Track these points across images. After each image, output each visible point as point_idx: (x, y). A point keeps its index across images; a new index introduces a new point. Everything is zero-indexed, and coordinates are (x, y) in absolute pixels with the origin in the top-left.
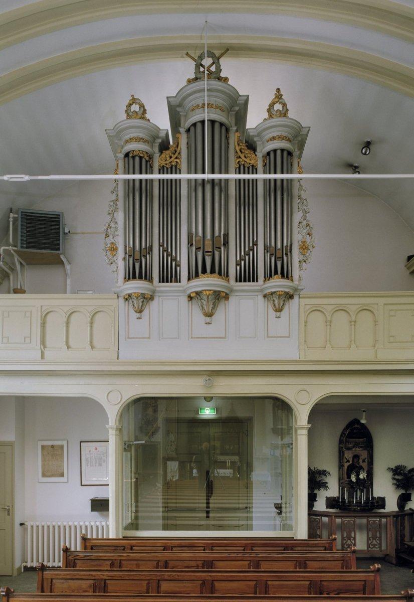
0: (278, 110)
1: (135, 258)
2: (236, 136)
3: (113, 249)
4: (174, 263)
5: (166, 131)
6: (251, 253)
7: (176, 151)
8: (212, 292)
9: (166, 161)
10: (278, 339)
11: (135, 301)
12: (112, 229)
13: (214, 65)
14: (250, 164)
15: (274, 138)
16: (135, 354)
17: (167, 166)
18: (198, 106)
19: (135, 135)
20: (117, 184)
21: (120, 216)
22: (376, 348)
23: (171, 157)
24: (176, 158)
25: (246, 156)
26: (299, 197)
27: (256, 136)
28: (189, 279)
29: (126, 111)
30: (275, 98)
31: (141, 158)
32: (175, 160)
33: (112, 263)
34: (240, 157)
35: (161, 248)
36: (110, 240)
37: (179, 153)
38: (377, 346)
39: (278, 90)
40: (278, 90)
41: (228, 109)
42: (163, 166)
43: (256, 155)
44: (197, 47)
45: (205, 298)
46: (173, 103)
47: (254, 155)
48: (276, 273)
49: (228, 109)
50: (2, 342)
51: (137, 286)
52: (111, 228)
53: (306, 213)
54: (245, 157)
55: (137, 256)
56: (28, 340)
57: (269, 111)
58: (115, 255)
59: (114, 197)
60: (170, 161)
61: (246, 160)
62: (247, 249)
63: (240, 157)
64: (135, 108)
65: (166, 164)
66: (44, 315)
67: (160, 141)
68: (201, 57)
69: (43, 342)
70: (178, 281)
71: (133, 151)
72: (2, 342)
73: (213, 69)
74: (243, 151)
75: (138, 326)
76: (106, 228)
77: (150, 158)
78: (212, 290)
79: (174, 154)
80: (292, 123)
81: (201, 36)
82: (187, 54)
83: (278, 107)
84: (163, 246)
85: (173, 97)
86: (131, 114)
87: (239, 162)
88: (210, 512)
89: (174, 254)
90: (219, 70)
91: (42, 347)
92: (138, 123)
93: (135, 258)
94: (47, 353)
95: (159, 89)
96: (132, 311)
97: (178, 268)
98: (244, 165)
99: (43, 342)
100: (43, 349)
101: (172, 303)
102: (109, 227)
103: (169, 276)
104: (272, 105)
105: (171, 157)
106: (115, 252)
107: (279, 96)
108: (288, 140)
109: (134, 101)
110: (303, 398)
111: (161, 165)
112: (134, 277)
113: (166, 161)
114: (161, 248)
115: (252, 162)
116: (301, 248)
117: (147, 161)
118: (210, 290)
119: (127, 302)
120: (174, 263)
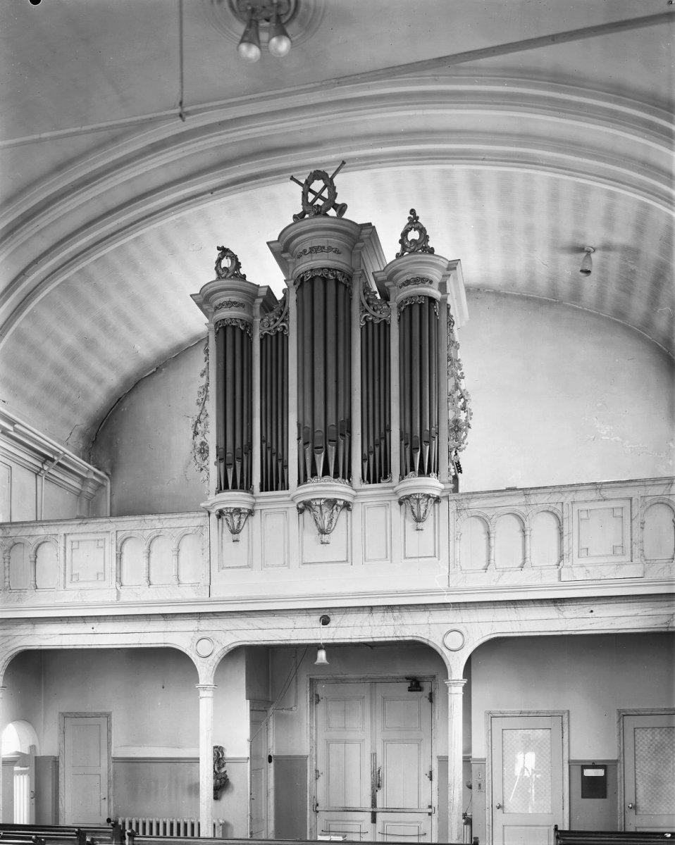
0: (413, 240)
1: (227, 463)
2: (361, 283)
3: (203, 450)
4: (280, 464)
5: (266, 289)
6: (383, 442)
7: (282, 312)
8: (322, 501)
9: (269, 326)
10: (420, 560)
11: (229, 518)
12: (203, 424)
13: (326, 189)
14: (380, 319)
15: (314, 250)
16: (232, 587)
17: (272, 334)
18: (305, 251)
19: (226, 299)
20: (208, 363)
21: (211, 407)
22: (560, 567)
23: (275, 321)
24: (283, 321)
25: (375, 308)
26: (449, 359)
27: (386, 281)
28: (299, 483)
29: (216, 268)
30: (408, 224)
31: (234, 327)
32: (281, 325)
33: (202, 470)
34: (367, 311)
35: (264, 445)
36: (199, 439)
37: (286, 314)
38: (561, 564)
39: (412, 212)
40: (412, 212)
41: (347, 248)
42: (266, 334)
43: (388, 306)
44: (656, 297)
45: (318, 509)
46: (380, 279)
47: (386, 307)
48: (413, 469)
49: (347, 248)
50: (72, 580)
51: (235, 499)
52: (200, 423)
53: (459, 378)
54: (374, 310)
55: (230, 461)
56: (101, 578)
57: (401, 242)
58: (206, 459)
59: (203, 381)
60: (275, 326)
61: (374, 313)
62: (377, 437)
63: (367, 311)
64: (226, 263)
65: (270, 331)
66: (119, 545)
67: (261, 300)
68: (308, 183)
69: (119, 579)
70: (274, 488)
71: (224, 320)
72: (72, 580)
73: (325, 194)
74: (371, 302)
75: (235, 552)
76: (194, 423)
77: (247, 326)
78: (324, 498)
79: (280, 316)
80: (336, 223)
81: (182, 108)
82: (292, 178)
83: (414, 235)
84: (266, 441)
85: (275, 242)
86: (221, 271)
87: (365, 317)
88: (87, 833)
89: (274, 447)
90: (333, 194)
91: (118, 585)
92: (227, 284)
93: (227, 463)
94: (122, 591)
95: (252, 232)
96: (227, 530)
97: (285, 470)
98: (372, 321)
99: (119, 579)
100: (119, 588)
101: (275, 517)
102: (199, 421)
103: (274, 481)
104: (405, 234)
105: (275, 321)
106: (206, 454)
107: (414, 221)
108: (337, 252)
109: (224, 252)
110: (205, 645)
111: (263, 333)
112: (226, 487)
113: (269, 326)
114: (264, 445)
115: (384, 316)
116: (451, 430)
117: (242, 332)
118: (321, 499)
119: (220, 521)
120: (280, 464)
